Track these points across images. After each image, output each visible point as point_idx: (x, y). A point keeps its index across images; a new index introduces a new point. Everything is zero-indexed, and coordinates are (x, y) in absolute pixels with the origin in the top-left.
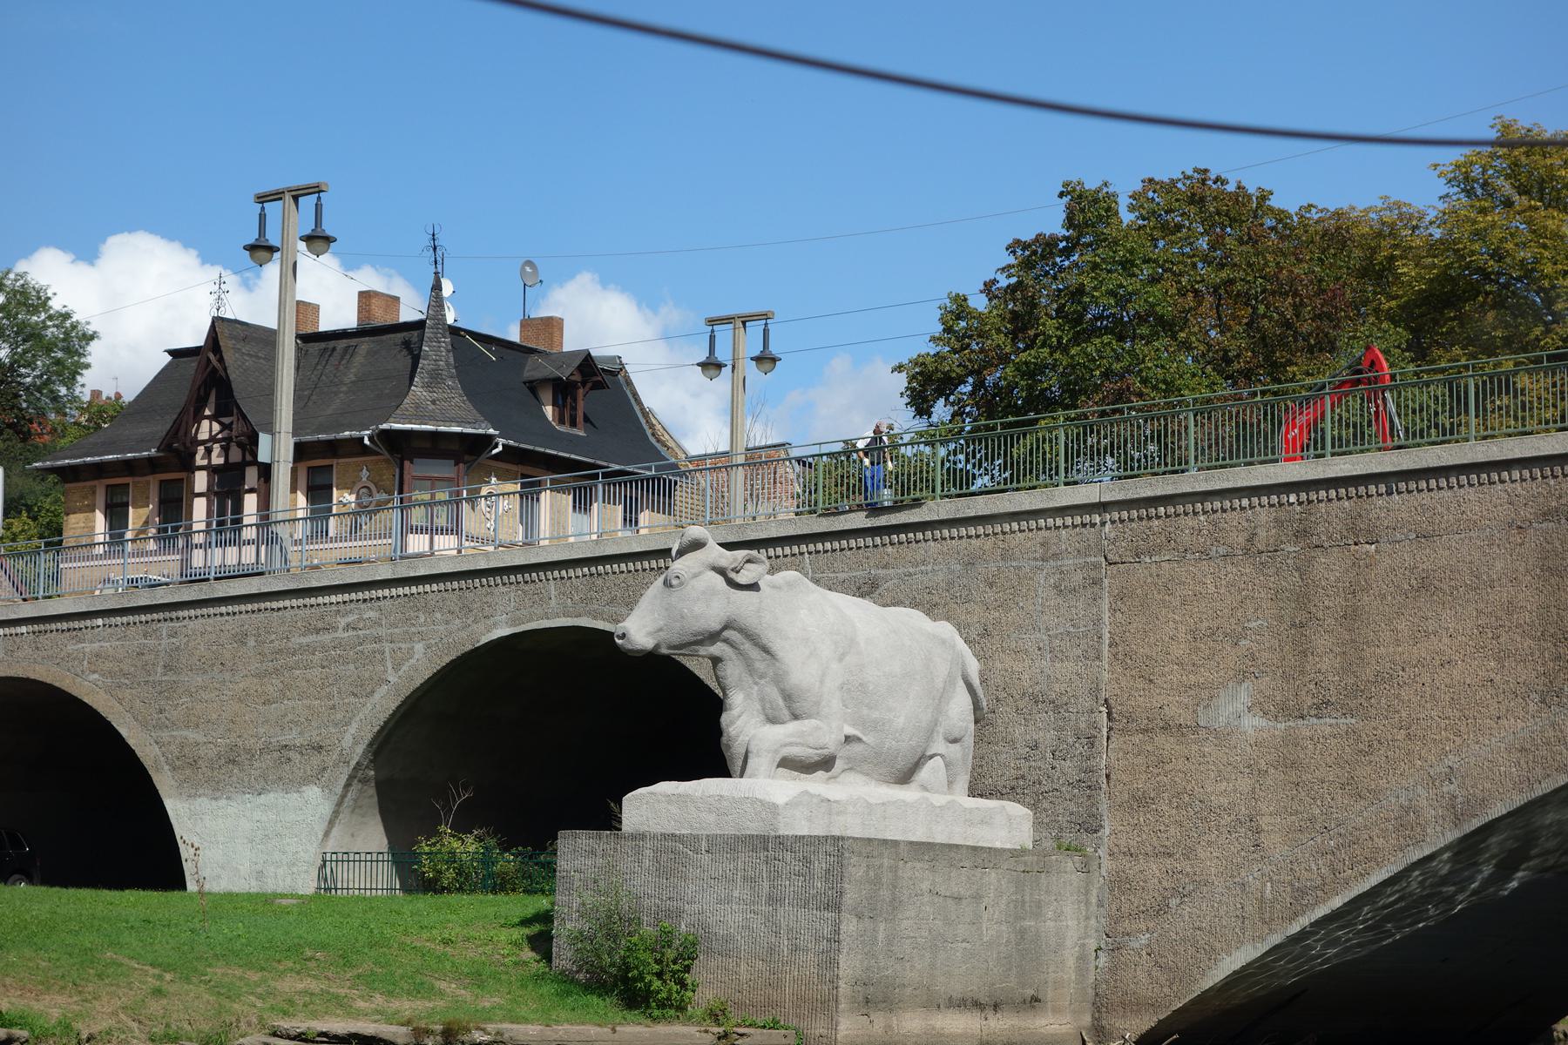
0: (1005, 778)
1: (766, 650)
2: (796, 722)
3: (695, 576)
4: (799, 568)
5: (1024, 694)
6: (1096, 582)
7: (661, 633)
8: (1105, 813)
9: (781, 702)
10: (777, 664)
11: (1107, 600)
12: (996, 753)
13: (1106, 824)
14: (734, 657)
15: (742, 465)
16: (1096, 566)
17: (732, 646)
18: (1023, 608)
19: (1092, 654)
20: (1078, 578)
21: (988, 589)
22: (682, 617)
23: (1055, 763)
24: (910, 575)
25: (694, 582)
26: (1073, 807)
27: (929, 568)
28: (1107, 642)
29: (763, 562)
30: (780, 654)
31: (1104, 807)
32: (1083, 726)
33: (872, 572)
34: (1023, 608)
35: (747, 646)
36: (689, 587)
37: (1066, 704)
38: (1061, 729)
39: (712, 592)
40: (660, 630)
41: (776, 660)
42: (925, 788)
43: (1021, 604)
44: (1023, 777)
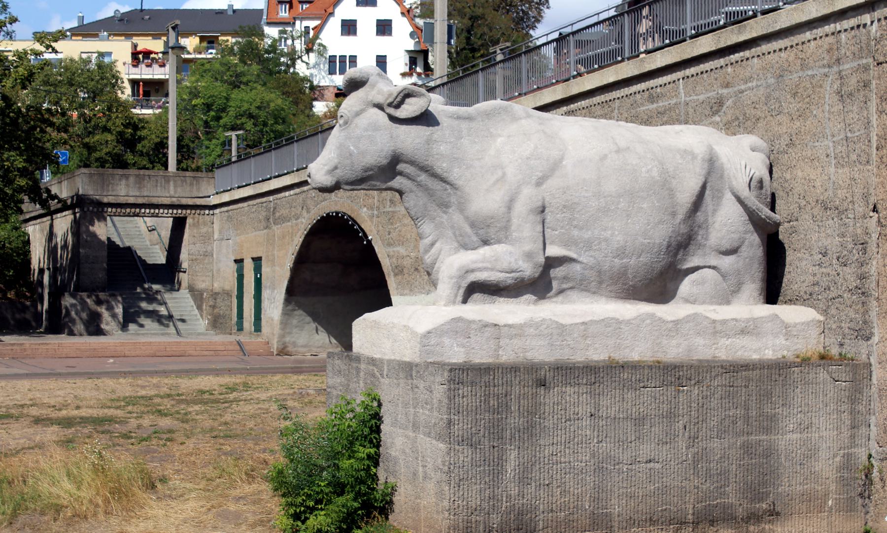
0: (806, 284)
1: (443, 180)
2: (487, 248)
3: (358, 114)
4: (491, 94)
5: (817, 201)
6: (866, 85)
7: (338, 171)
8: (875, 320)
9: (468, 230)
10: (459, 193)
11: (874, 102)
12: (800, 260)
13: (876, 331)
14: (414, 188)
15: (627, 12)
16: (866, 68)
17: (410, 179)
18: (815, 116)
19: (864, 159)
20: (853, 81)
21: (792, 100)
22: (351, 155)
23: (839, 269)
24: (742, 92)
25: (358, 121)
26: (852, 314)
27: (754, 84)
28: (875, 146)
29: (423, 95)
30: (460, 183)
31: (873, 314)
32: (859, 231)
33: (720, 92)
34: (815, 116)
35: (423, 177)
36: (353, 126)
37: (846, 210)
38: (843, 235)
39: (375, 127)
40: (336, 168)
41: (456, 189)
42: (687, 301)
43: (815, 112)
44: (817, 284)
